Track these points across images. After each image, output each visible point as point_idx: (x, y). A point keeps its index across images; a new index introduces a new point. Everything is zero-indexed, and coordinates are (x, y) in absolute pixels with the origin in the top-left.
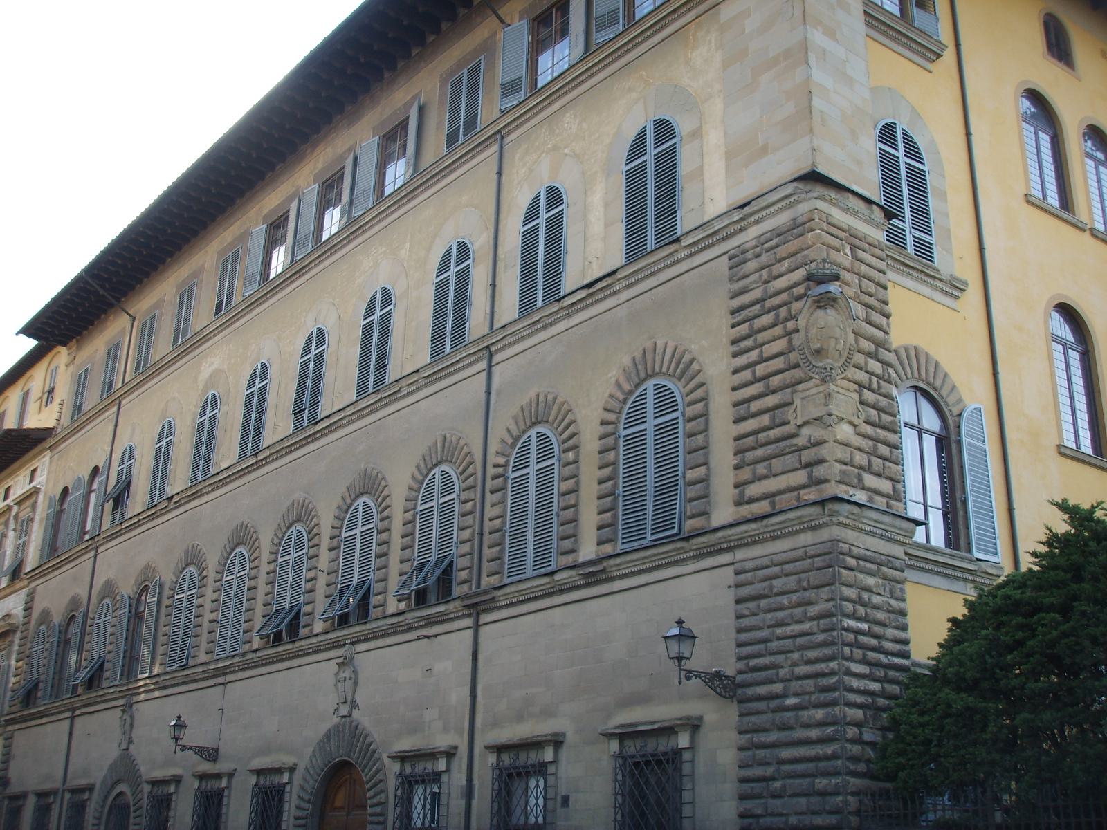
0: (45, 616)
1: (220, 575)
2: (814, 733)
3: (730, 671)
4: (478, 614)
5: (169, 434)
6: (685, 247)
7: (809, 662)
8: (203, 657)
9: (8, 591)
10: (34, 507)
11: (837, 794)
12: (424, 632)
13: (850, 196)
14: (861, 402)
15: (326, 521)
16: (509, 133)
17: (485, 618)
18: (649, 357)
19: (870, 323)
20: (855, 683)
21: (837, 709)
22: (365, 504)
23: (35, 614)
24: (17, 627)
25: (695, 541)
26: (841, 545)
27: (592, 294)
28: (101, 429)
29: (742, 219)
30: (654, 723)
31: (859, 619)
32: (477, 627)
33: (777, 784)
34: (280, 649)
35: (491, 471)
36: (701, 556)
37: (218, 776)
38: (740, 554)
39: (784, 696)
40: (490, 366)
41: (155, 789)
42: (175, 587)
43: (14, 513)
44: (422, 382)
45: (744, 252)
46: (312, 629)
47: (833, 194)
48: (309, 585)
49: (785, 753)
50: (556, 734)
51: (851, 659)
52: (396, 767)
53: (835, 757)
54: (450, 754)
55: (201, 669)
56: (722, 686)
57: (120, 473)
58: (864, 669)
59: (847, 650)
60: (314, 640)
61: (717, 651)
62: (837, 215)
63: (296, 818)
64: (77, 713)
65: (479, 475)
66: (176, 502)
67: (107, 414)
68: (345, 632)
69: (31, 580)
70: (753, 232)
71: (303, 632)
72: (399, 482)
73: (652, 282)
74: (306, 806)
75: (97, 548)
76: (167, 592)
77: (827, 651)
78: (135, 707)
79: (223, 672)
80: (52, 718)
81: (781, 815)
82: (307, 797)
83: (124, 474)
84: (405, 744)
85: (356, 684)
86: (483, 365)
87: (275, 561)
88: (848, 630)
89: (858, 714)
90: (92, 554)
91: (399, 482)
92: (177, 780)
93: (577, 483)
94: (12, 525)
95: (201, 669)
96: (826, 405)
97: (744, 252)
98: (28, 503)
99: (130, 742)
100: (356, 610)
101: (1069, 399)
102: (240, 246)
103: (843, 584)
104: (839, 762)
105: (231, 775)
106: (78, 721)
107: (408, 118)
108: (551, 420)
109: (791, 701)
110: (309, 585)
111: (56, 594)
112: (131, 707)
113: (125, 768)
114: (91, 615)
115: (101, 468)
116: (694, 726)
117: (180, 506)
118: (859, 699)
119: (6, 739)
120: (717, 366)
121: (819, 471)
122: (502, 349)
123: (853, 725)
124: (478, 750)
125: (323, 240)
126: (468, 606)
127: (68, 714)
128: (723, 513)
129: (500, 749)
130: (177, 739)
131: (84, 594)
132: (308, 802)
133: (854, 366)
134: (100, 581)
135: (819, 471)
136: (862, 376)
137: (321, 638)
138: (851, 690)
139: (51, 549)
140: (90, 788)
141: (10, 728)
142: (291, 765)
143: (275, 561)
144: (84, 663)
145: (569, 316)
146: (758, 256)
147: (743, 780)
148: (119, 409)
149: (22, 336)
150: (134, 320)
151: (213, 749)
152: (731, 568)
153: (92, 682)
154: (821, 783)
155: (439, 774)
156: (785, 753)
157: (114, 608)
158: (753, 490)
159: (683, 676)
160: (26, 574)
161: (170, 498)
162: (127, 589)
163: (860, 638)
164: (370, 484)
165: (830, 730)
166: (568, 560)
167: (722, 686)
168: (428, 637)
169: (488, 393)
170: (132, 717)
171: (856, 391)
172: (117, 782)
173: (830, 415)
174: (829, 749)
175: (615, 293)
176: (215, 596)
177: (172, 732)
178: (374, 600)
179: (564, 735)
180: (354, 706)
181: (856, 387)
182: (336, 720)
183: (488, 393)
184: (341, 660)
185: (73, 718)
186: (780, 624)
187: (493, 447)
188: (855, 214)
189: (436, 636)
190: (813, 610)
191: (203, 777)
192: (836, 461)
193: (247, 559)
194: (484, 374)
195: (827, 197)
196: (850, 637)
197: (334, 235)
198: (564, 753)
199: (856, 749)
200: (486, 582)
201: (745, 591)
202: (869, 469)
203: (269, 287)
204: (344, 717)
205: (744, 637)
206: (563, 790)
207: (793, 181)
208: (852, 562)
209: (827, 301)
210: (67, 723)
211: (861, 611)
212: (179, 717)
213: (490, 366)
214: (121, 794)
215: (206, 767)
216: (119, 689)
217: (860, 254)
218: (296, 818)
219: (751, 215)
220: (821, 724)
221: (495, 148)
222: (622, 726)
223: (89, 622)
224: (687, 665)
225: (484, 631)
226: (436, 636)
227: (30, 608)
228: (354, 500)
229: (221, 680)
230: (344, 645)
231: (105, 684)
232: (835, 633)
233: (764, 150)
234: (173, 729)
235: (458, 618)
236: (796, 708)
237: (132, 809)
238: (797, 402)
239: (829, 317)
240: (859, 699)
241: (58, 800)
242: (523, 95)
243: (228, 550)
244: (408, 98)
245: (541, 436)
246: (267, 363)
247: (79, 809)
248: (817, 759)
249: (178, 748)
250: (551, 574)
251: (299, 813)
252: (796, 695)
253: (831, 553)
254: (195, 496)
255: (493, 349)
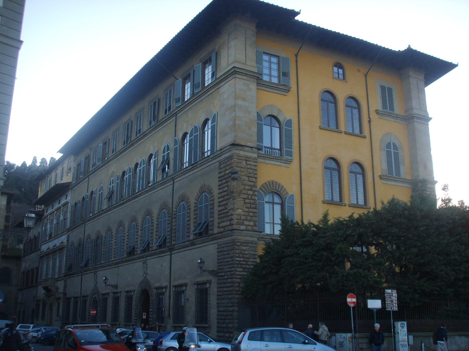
0: (73, 243)
1: (142, 225)
2: (229, 285)
3: (216, 270)
4: (171, 251)
5: (102, 190)
6: (211, 158)
7: (229, 268)
8: (113, 259)
9: (49, 241)
10: (67, 208)
11: (233, 299)
12: (161, 255)
13: (245, 147)
14: (245, 203)
15: (140, 221)
16: (178, 114)
17: (173, 252)
18: (203, 186)
19: (249, 181)
20: (238, 273)
21: (233, 279)
22: (183, 204)
23: (70, 243)
24: (65, 246)
25: (210, 237)
26: (236, 240)
27: (193, 167)
28: (84, 185)
29: (220, 153)
30: (202, 281)
31: (241, 258)
32: (171, 255)
33: (223, 296)
34: (130, 258)
35: (174, 213)
36: (211, 240)
37: (117, 293)
38: (219, 241)
39: (224, 276)
40: (173, 183)
41: (199, 287)
42: (159, 218)
43: (62, 209)
44: (159, 185)
45: (221, 162)
46: (138, 252)
47: (240, 148)
48: (136, 240)
49: (225, 289)
50: (185, 283)
51: (237, 267)
52: (155, 291)
53: (232, 290)
54: (166, 288)
55: (112, 262)
56: (214, 273)
57: (164, 156)
58: (242, 270)
59: (236, 266)
60: (137, 256)
61: (211, 264)
62: (242, 153)
63: (135, 304)
64: (83, 273)
65: (171, 213)
66: (104, 212)
67: (86, 180)
68: (144, 254)
69: (68, 231)
70: (223, 156)
71: (210, 232)
72: (155, 212)
73: (205, 166)
74: (137, 301)
75: (85, 223)
76: (104, 239)
77: (232, 266)
78: (97, 272)
79: (117, 263)
80: (77, 275)
81: (224, 304)
82: (137, 299)
83: (166, 157)
84: (157, 285)
85: (147, 268)
86: (172, 182)
87: (129, 232)
88: (237, 260)
89: (239, 280)
90: (84, 225)
91: (155, 212)
92: (108, 294)
93: (190, 218)
94: (55, 217)
95: (112, 262)
96: (234, 205)
97: (221, 162)
98: (66, 206)
99: (97, 283)
100: (147, 248)
101: (355, 187)
102: (142, 112)
103: (236, 250)
104: (233, 292)
105: (121, 292)
106: (83, 276)
107: (211, 57)
108: (206, 191)
109: (226, 277)
110: (136, 240)
111: (76, 236)
112: (96, 272)
113: (96, 290)
114: (85, 244)
115: (77, 202)
116: (210, 282)
117: (106, 213)
118: (239, 277)
119: (64, 281)
120: (216, 192)
121: (232, 222)
122: (177, 178)
123: (237, 283)
124: (171, 286)
125: (185, 101)
126: (169, 249)
127: (81, 274)
128: (216, 230)
129: (175, 287)
130: (105, 283)
131: (82, 237)
132: (138, 300)
133: (242, 194)
134: (86, 234)
135: (232, 222)
136: (245, 196)
137: (139, 255)
138: (237, 275)
139: (73, 221)
140: (87, 296)
141: (65, 278)
142: (133, 290)
143: (129, 232)
144: (84, 259)
145: (189, 172)
146: (224, 163)
147: (218, 295)
148: (89, 179)
149: (59, 153)
150: (91, 150)
151: (116, 285)
152: (216, 244)
153: (86, 265)
154: (230, 296)
155: (184, 291)
156: (225, 289)
157: (136, 226)
158: (221, 225)
159: (202, 272)
160: (67, 229)
161: (103, 210)
162: (94, 237)
163: (241, 262)
164: (149, 213)
165: (232, 284)
166: (188, 239)
167: (214, 273)
168: (162, 257)
169: (173, 190)
170: (97, 275)
171: (243, 200)
172: (94, 294)
173: (235, 208)
174: (231, 289)
175: (198, 168)
176: (115, 241)
177: (199, 265)
178: (151, 245)
179: (187, 283)
180: (147, 274)
181: (243, 199)
182: (143, 278)
183: (173, 190)
184: (143, 262)
185: (82, 275)
186: (225, 258)
187: (174, 206)
188: (248, 151)
189: (163, 256)
190: (230, 256)
191: (114, 293)
192: (236, 219)
193: (186, 206)
194: (172, 185)
195: (238, 149)
196: (238, 262)
197: (188, 99)
198: (188, 287)
199: (237, 289)
200: (173, 243)
201: (220, 250)
202: (246, 220)
203: (186, 105)
204: (145, 277)
205: (219, 261)
206: (187, 297)
207: (229, 145)
208: (238, 244)
209: (234, 179)
210: (80, 277)
211: (241, 255)
212: (106, 277)
213: (173, 183)
214: (95, 297)
215: (115, 290)
216: (93, 267)
217: (248, 162)
218: (135, 304)
219: (223, 152)
220: (230, 283)
221: (174, 118)
222: (197, 282)
223: (84, 246)
224: (107, 284)
225: (172, 255)
226: (163, 256)
227: (68, 240)
228: (180, 203)
229: (117, 265)
230: (144, 258)
231: (89, 265)
232: (233, 262)
233: (226, 134)
234: (199, 264)
235: (167, 252)
236: (227, 279)
237: (98, 302)
238: (229, 204)
239: (234, 183)
240: (239, 277)
241: (80, 299)
242: (200, 89)
243: (199, 194)
244: (156, 95)
245: (183, 204)
246: (169, 145)
247: (85, 302)
248: (229, 291)
249: (202, 271)
250: (184, 242)
251: (136, 303)
252: (227, 276)
253: (233, 242)
254: (109, 210)
255: (174, 178)
